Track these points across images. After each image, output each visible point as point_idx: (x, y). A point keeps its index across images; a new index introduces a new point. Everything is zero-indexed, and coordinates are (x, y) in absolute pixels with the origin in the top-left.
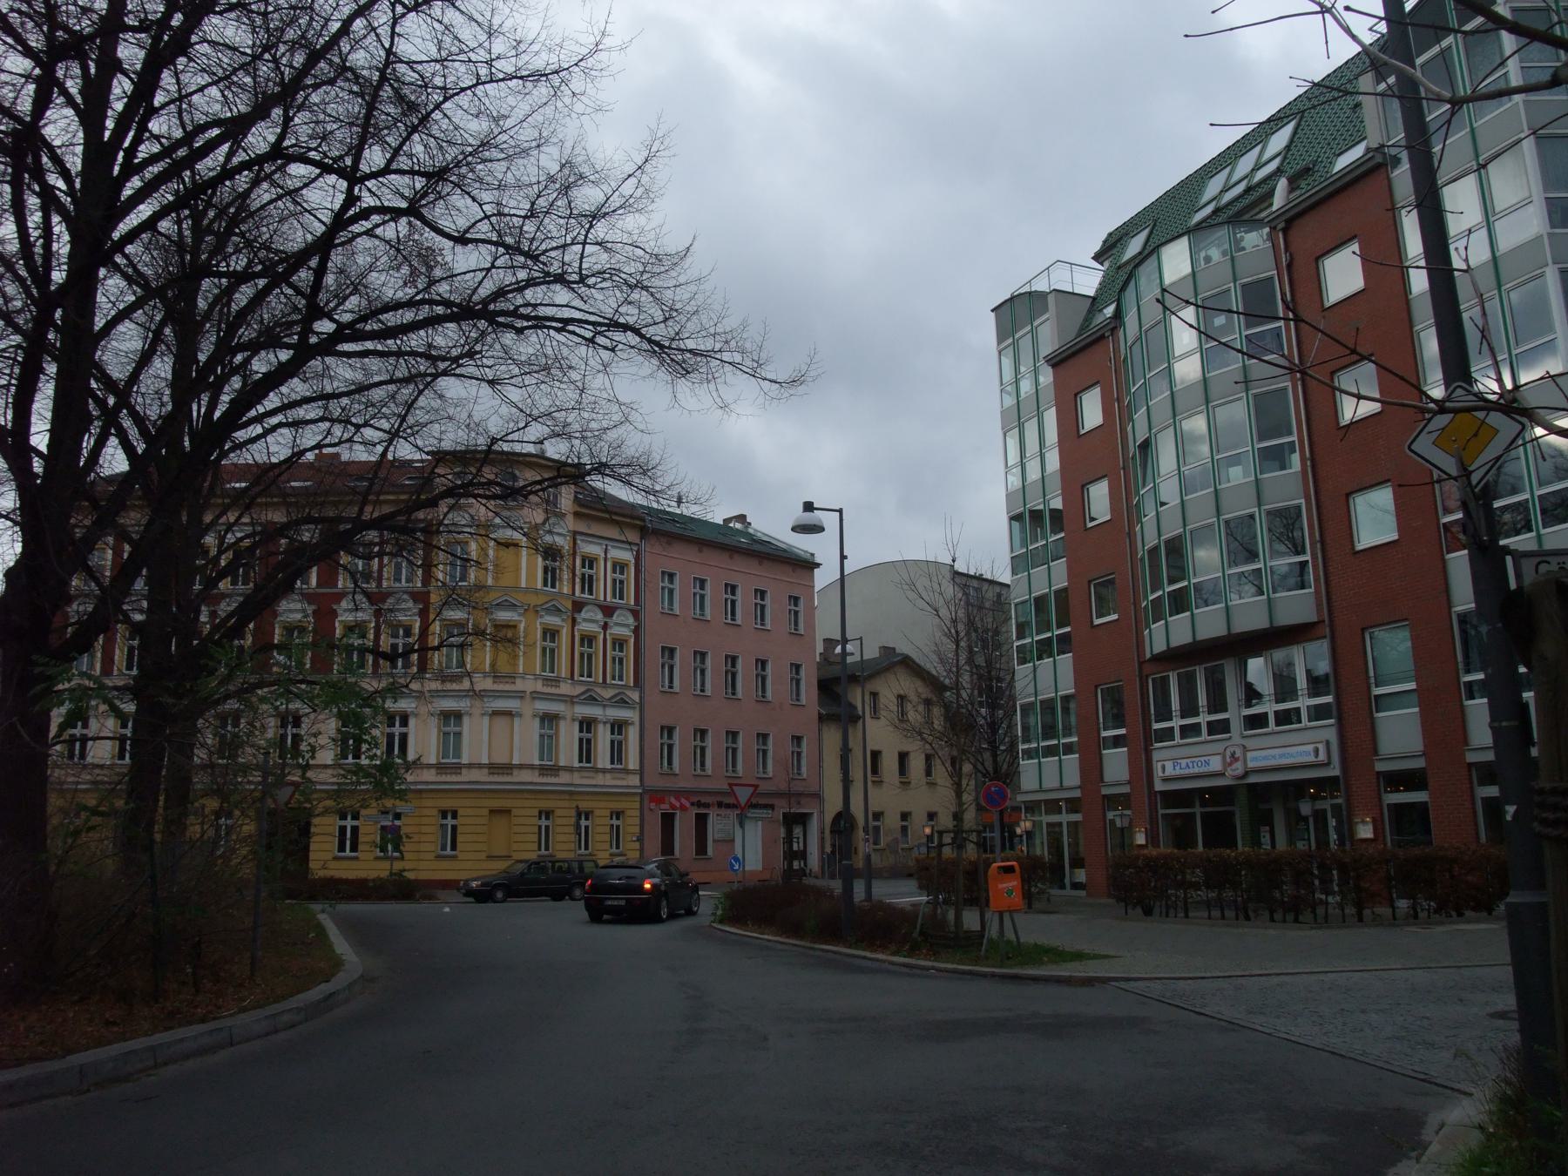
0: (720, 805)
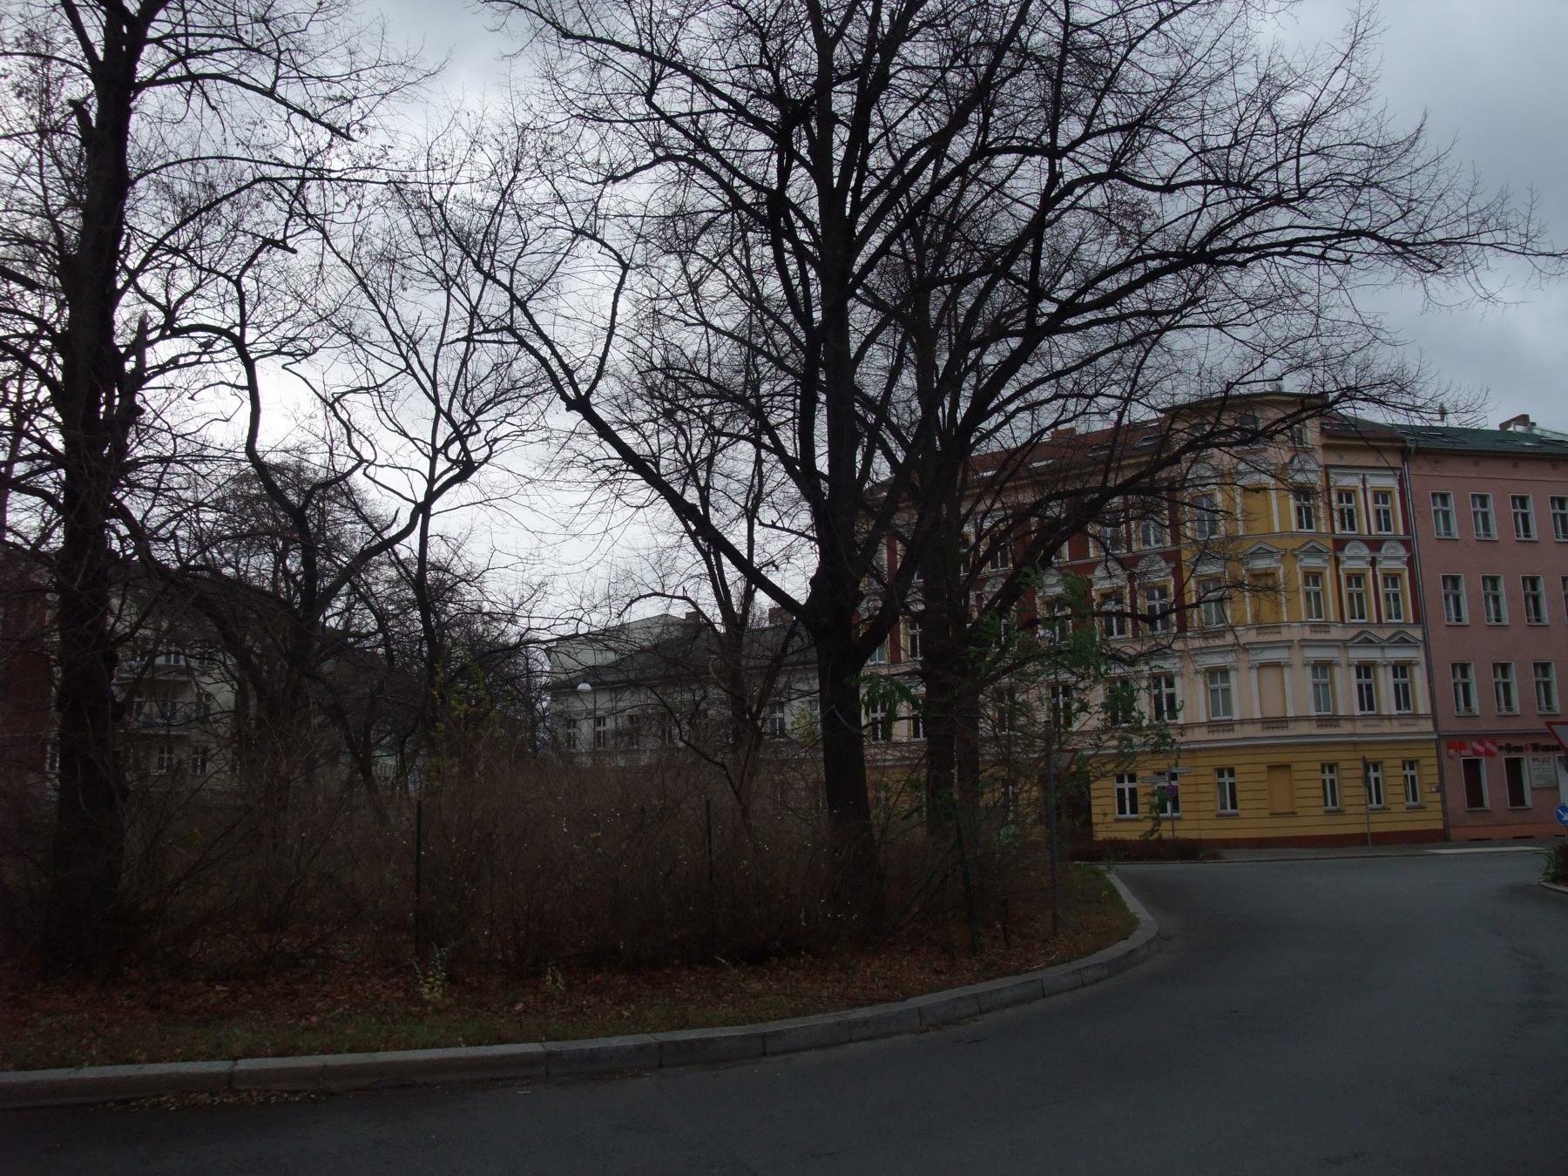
0: (1535, 748)
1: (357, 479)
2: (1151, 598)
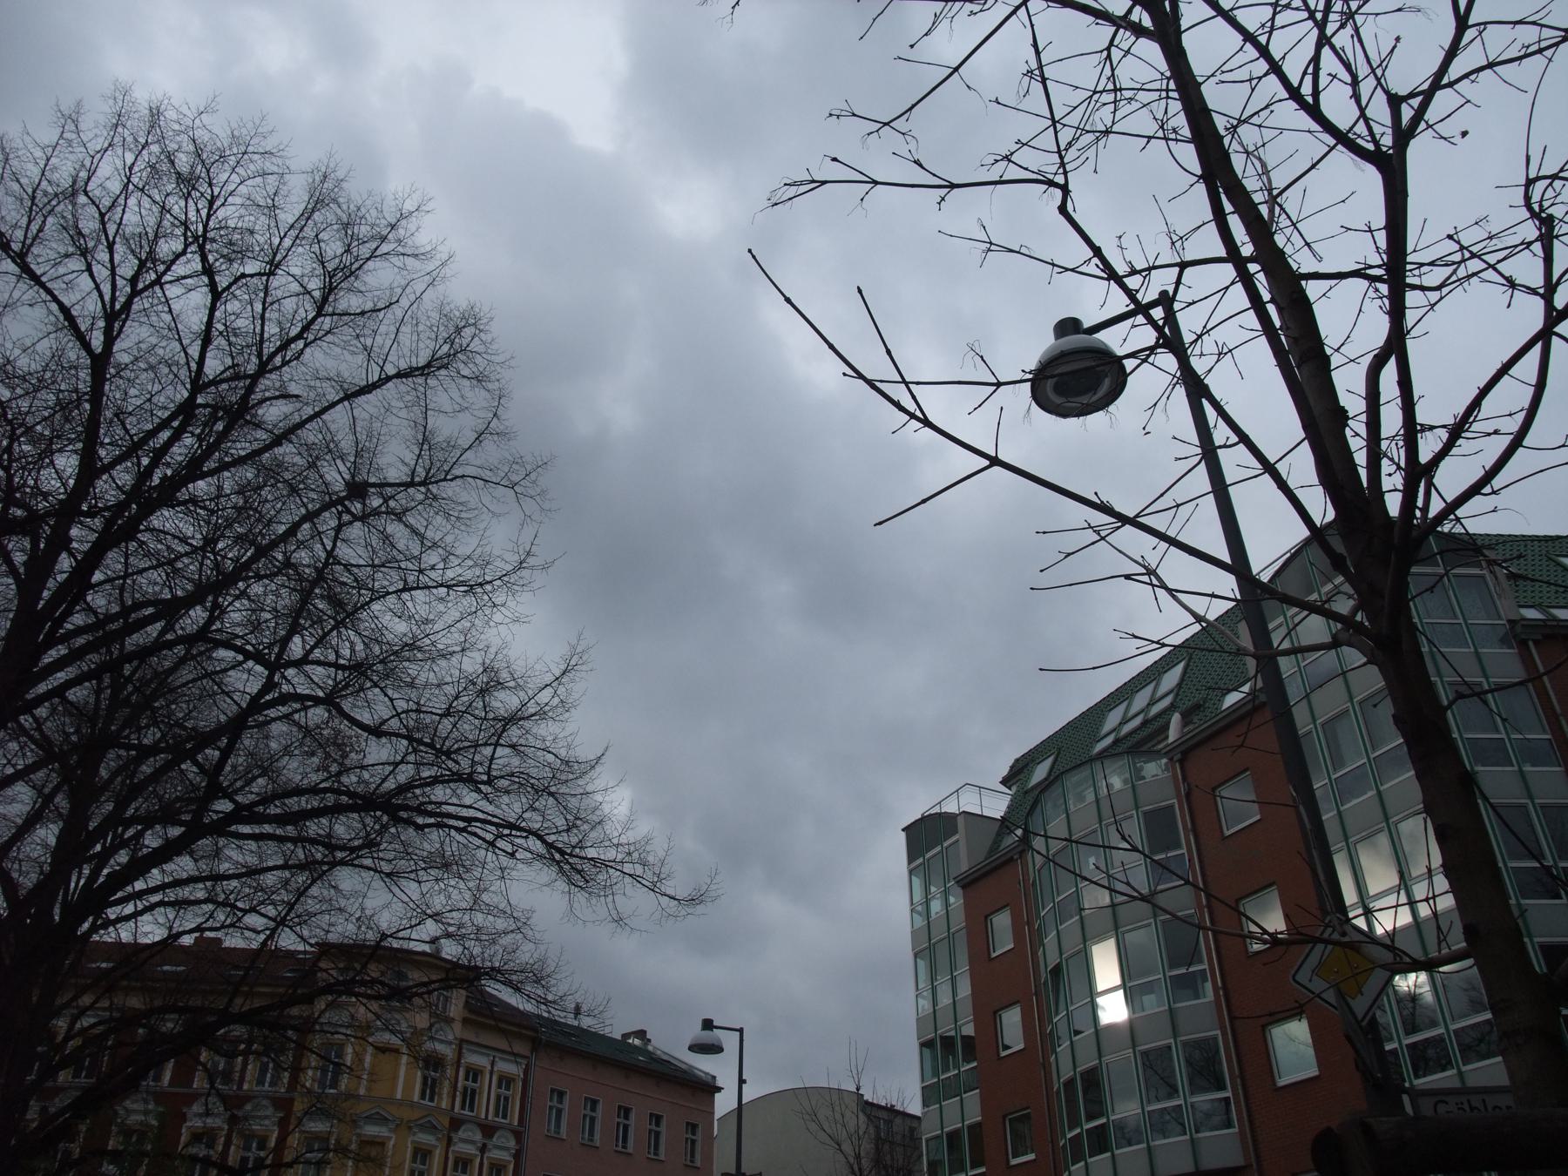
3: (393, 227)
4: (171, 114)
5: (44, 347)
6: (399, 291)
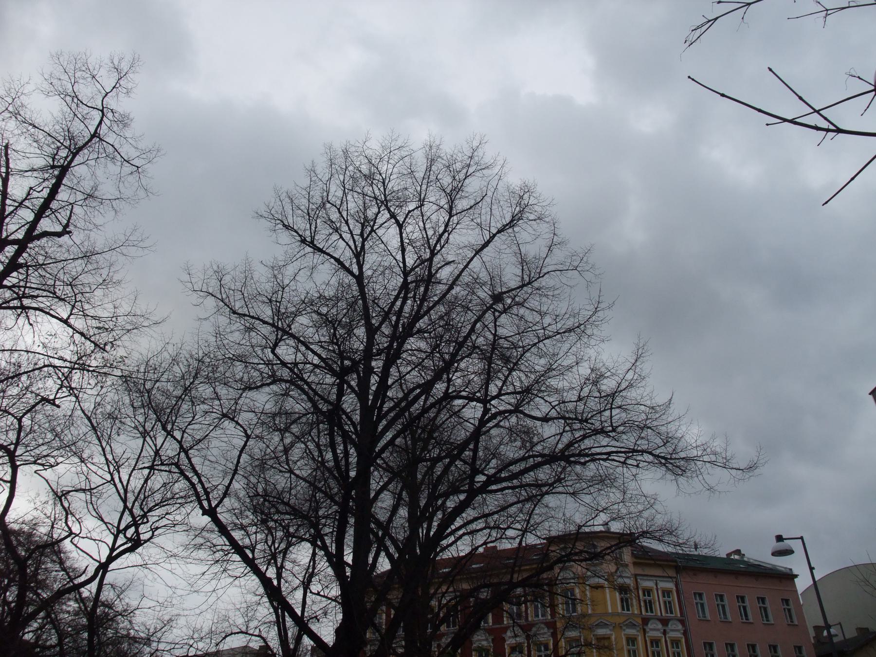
1: (67, 544)
2: (540, 651)
3: (471, 158)
4: (352, 149)
5: (334, 281)
6: (485, 189)
